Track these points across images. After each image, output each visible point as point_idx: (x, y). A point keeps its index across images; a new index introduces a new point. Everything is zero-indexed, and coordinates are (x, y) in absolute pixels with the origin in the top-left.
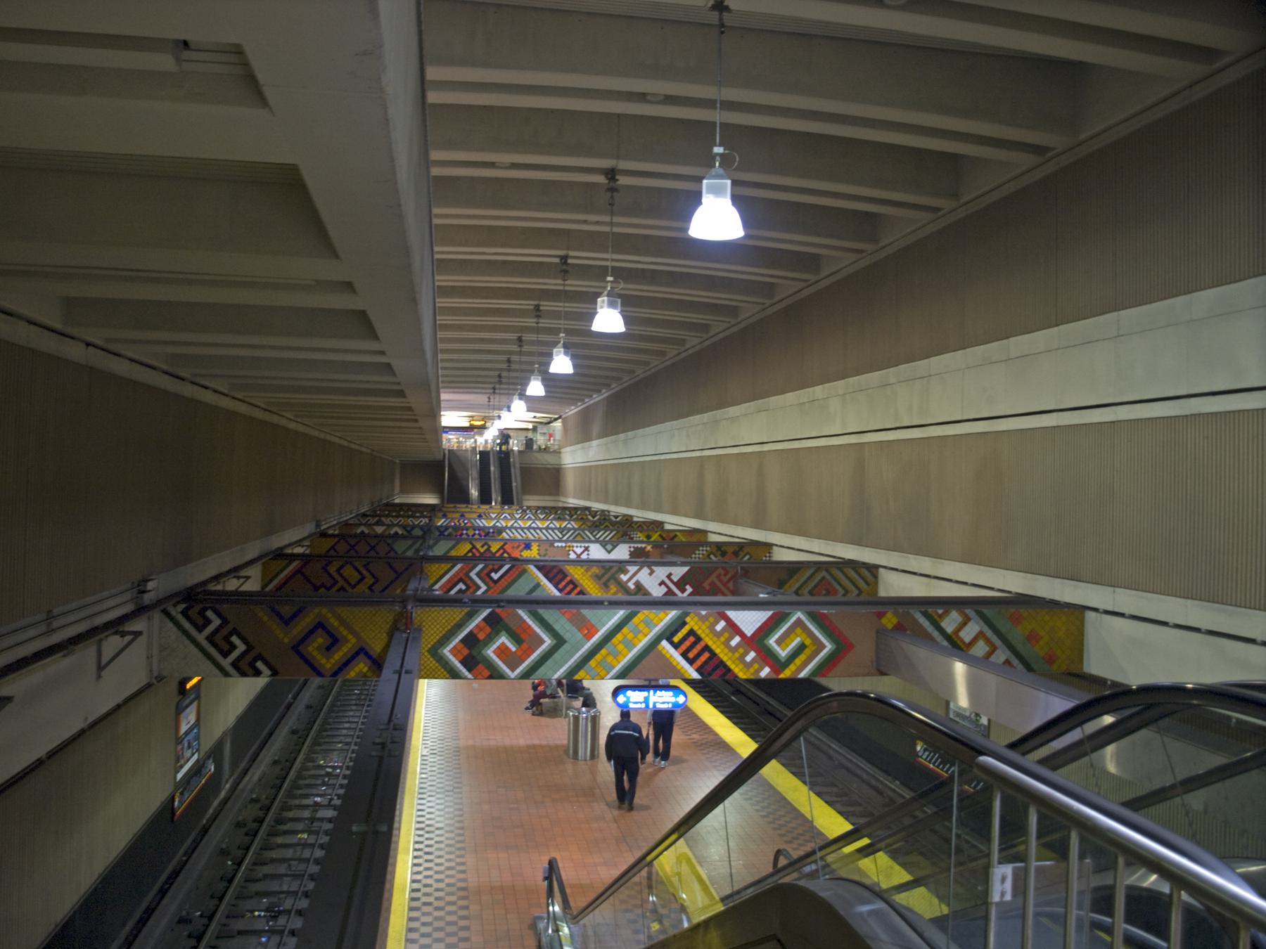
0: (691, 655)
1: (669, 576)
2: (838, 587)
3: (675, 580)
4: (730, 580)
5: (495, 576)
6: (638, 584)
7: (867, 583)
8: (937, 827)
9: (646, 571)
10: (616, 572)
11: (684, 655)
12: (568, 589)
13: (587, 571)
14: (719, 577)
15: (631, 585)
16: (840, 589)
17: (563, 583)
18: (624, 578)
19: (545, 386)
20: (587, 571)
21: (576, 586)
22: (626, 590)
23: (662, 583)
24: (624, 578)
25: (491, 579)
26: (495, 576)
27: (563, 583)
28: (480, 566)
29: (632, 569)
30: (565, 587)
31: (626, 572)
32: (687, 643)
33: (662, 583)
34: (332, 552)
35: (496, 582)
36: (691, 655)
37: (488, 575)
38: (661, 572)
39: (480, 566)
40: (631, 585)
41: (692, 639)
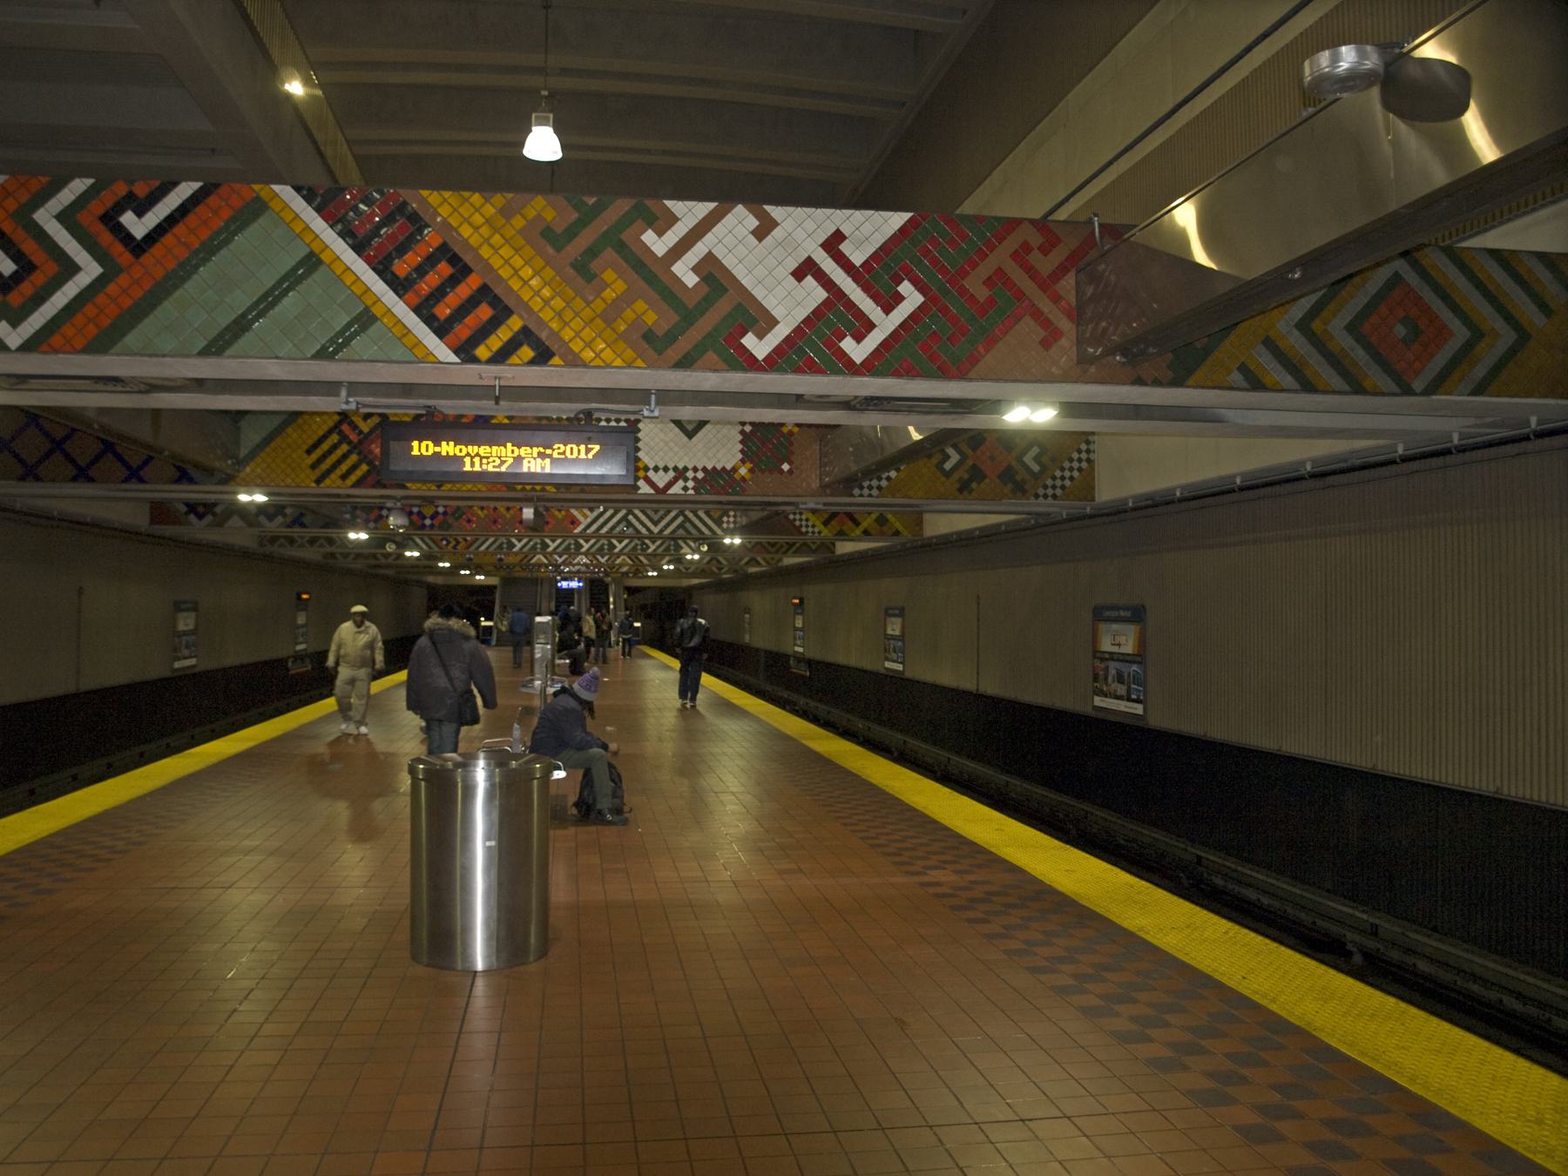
0: (444, 311)
1: (833, 244)
2: (1446, 315)
3: (858, 259)
4: (1062, 270)
5: (137, 226)
6: (711, 269)
7: (1544, 307)
8: (436, 549)
9: (740, 219)
10: (626, 222)
11: (423, 310)
12: (432, 280)
13: (507, 213)
14: (1021, 255)
15: (685, 272)
16: (1455, 324)
17: (413, 259)
18: (657, 244)
19: (1323, 49)
20: (507, 213)
21: (462, 269)
22: (667, 290)
23: (807, 269)
24: (657, 244)
25: (126, 237)
26: (137, 226)
27: (413, 259)
28: (79, 186)
29: (689, 212)
30: (421, 271)
31: (664, 222)
32: (432, 280)
33: (807, 269)
34: (681, 532)
35: (138, 248)
36: (444, 311)
37: (110, 218)
38: (804, 228)
39: (79, 186)
40: (685, 272)
41: (444, 269)
